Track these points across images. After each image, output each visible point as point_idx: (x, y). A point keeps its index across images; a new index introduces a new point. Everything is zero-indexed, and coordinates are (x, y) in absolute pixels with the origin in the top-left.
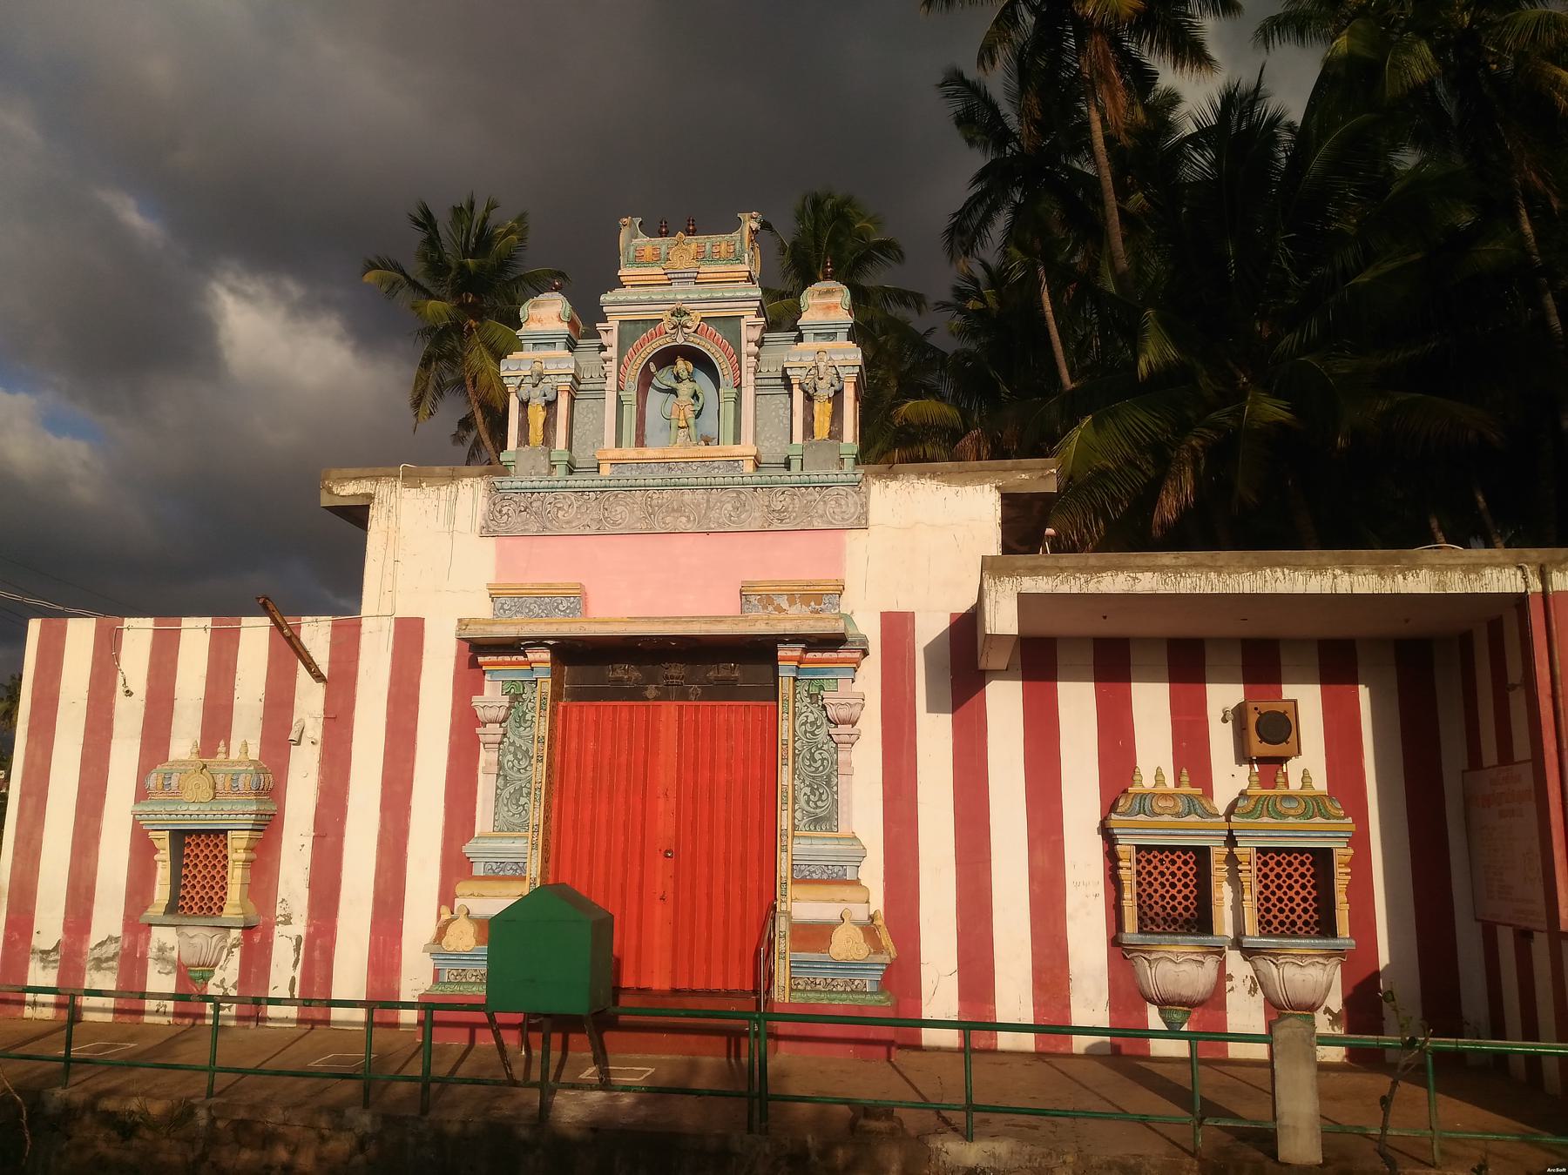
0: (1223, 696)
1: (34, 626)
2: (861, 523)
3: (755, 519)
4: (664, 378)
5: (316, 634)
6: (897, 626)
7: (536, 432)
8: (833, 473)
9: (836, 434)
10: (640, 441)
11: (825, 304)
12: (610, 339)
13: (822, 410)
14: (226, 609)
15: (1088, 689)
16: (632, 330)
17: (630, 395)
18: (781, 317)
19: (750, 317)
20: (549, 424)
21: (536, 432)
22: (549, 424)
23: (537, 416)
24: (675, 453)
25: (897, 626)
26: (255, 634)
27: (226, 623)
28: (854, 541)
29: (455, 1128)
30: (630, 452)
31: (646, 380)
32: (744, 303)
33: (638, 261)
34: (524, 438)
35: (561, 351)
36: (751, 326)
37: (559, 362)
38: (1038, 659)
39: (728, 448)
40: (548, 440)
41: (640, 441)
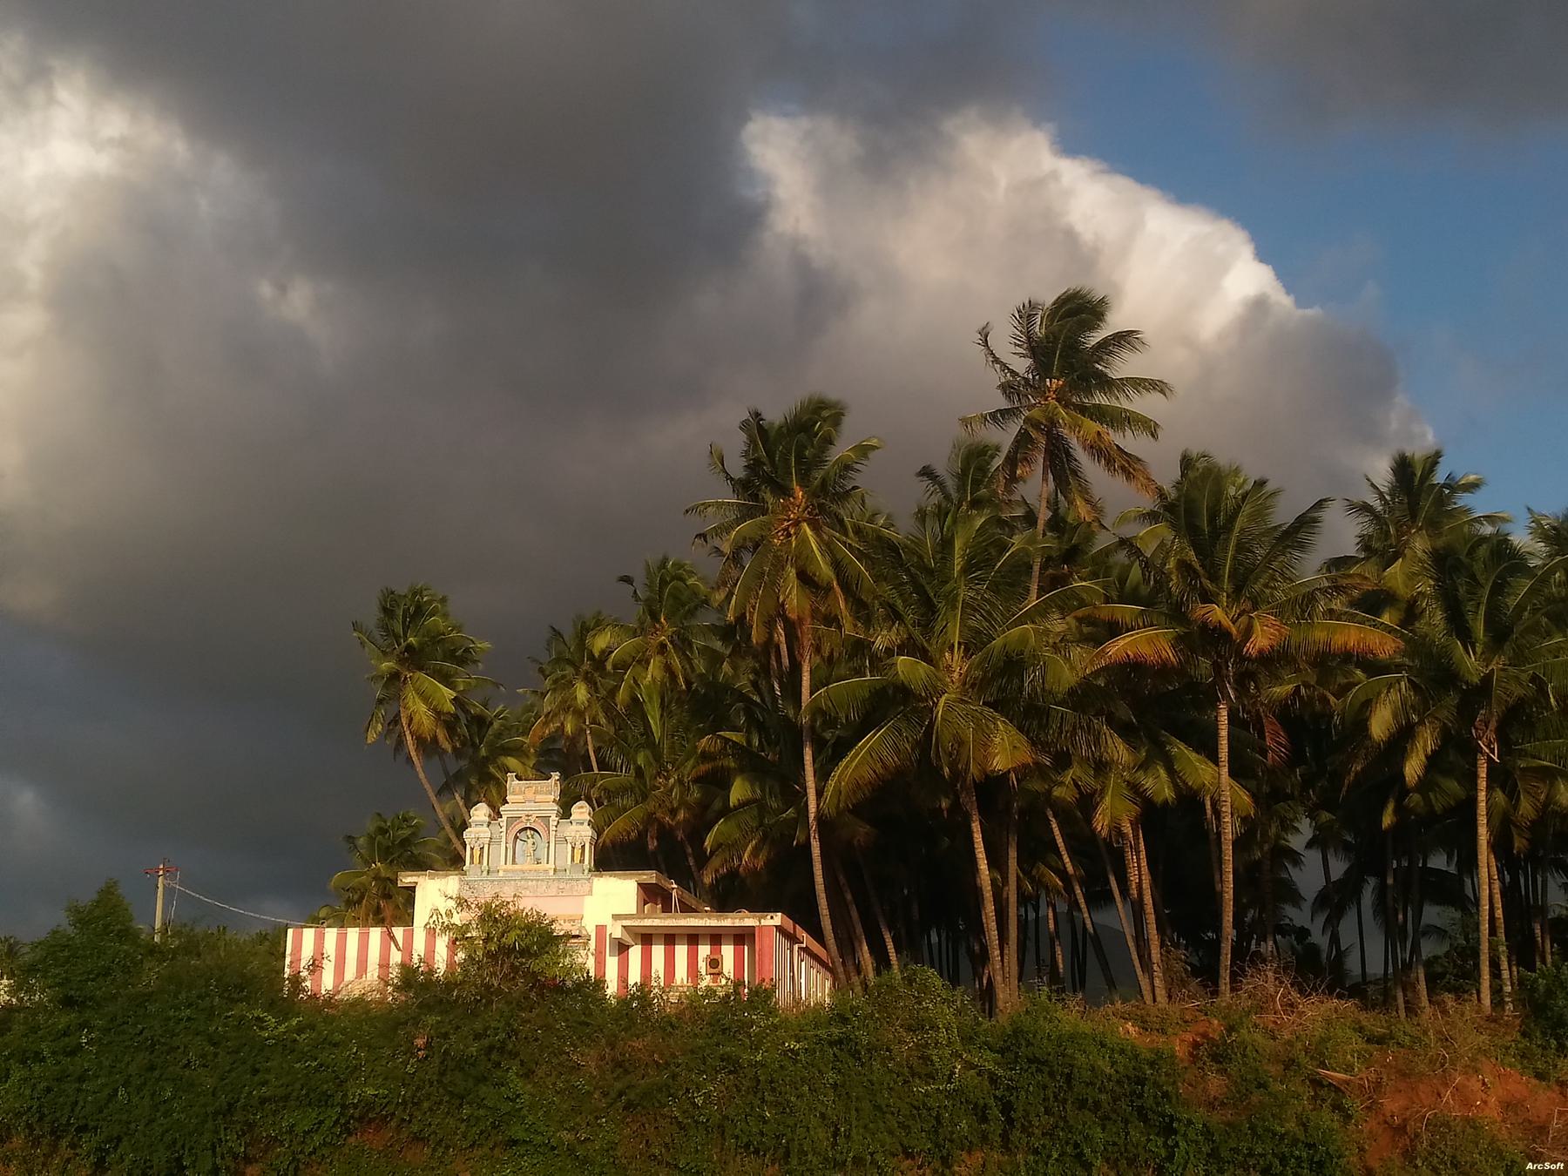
0: (704, 950)
1: (290, 931)
2: (590, 893)
3: (553, 891)
4: (522, 836)
5: (398, 932)
6: (601, 929)
7: (476, 860)
8: (581, 876)
9: (582, 861)
10: (514, 862)
11: (581, 811)
12: (504, 824)
13: (578, 852)
14: (342, 923)
15: (685, 947)
16: (511, 820)
17: (510, 846)
18: (565, 813)
19: (553, 817)
20: (481, 855)
21: (476, 860)
22: (481, 855)
23: (477, 853)
24: (526, 867)
25: (601, 929)
26: (376, 934)
27: (364, 930)
28: (588, 899)
29: (1029, 361)
30: (509, 866)
31: (516, 837)
32: (552, 810)
33: (514, 793)
34: (472, 862)
35: (485, 828)
36: (554, 818)
37: (484, 833)
38: (647, 938)
39: (544, 866)
40: (480, 862)
41: (514, 862)
